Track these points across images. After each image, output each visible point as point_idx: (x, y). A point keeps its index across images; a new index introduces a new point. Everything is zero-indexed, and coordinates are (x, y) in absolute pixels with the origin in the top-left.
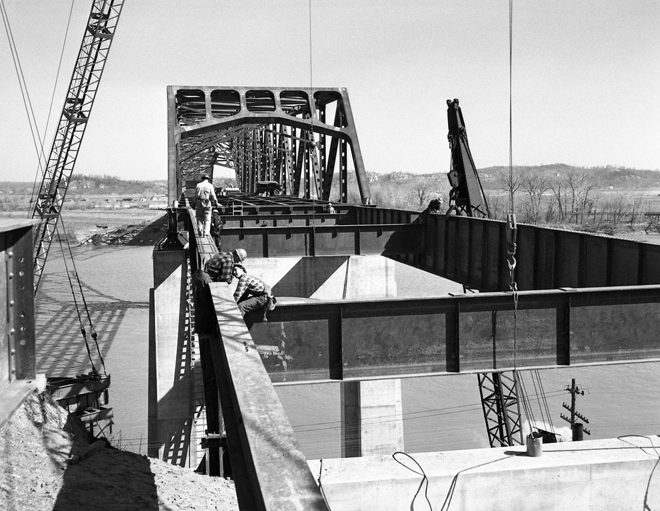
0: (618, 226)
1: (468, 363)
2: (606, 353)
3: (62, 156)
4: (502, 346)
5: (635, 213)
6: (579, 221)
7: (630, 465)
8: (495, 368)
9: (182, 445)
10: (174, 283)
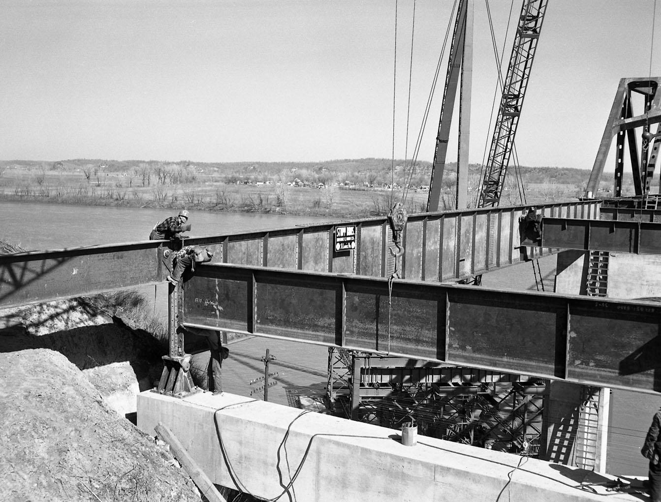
1: (353, 340)
2: (488, 357)
3: (508, 147)
4: (384, 330)
7: (476, 479)
8: (377, 350)
9: (570, 429)
10: (575, 271)
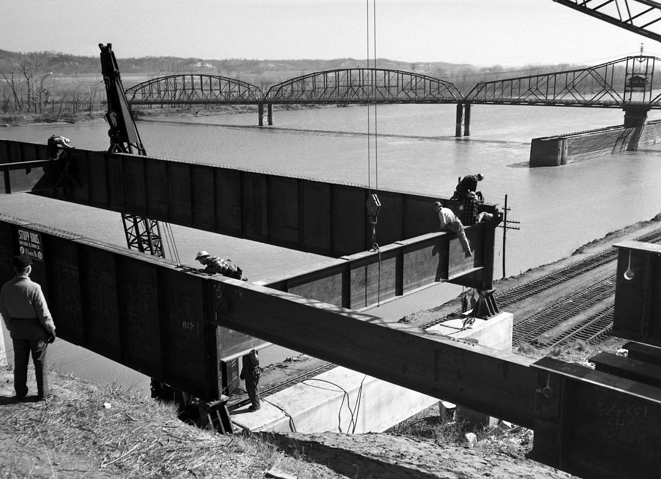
0: (77, 114)
5: (92, 102)
6: (38, 110)
